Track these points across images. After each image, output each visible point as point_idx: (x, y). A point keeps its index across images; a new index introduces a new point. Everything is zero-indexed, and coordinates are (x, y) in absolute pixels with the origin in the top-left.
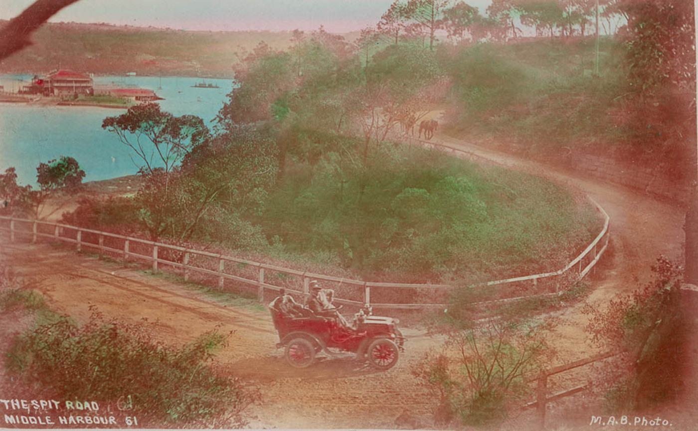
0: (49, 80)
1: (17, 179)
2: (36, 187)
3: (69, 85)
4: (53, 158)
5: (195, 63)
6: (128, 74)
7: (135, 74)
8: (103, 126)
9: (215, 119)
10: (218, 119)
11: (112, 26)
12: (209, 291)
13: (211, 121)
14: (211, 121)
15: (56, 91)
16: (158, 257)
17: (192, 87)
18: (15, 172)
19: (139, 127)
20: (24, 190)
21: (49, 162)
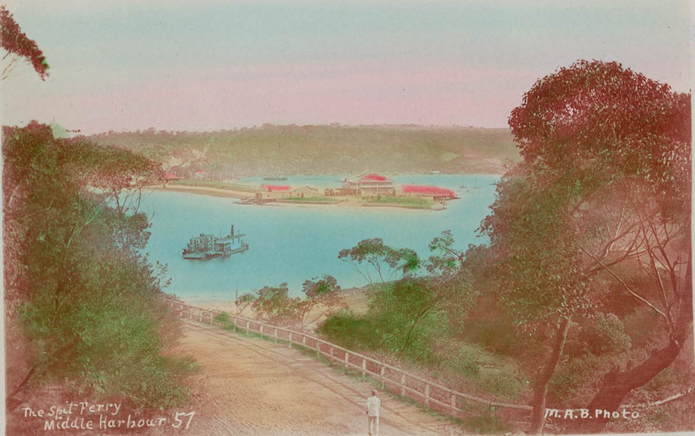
0: (357, 182)
1: (289, 292)
2: (303, 297)
3: (374, 186)
4: (318, 276)
5: (495, 160)
6: (432, 172)
7: (438, 172)
8: (339, 257)
9: (478, 229)
10: (481, 229)
11: (419, 126)
12: (394, 399)
13: (475, 231)
14: (475, 231)
15: (363, 192)
16: (349, 362)
17: (491, 184)
18: (287, 286)
19: (365, 258)
20: (294, 301)
21: (313, 279)
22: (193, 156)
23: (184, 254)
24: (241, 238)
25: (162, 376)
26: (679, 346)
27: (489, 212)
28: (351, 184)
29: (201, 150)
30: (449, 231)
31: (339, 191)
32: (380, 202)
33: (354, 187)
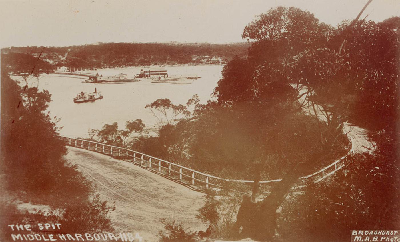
9: (212, 93)
22: (59, 59)
23: (74, 100)
24: (100, 93)
25: (85, 184)
26: (98, 132)
27: (217, 85)
28: (145, 72)
29: (63, 56)
30: (197, 95)
31: (138, 76)
32: (160, 81)
33: (146, 74)
